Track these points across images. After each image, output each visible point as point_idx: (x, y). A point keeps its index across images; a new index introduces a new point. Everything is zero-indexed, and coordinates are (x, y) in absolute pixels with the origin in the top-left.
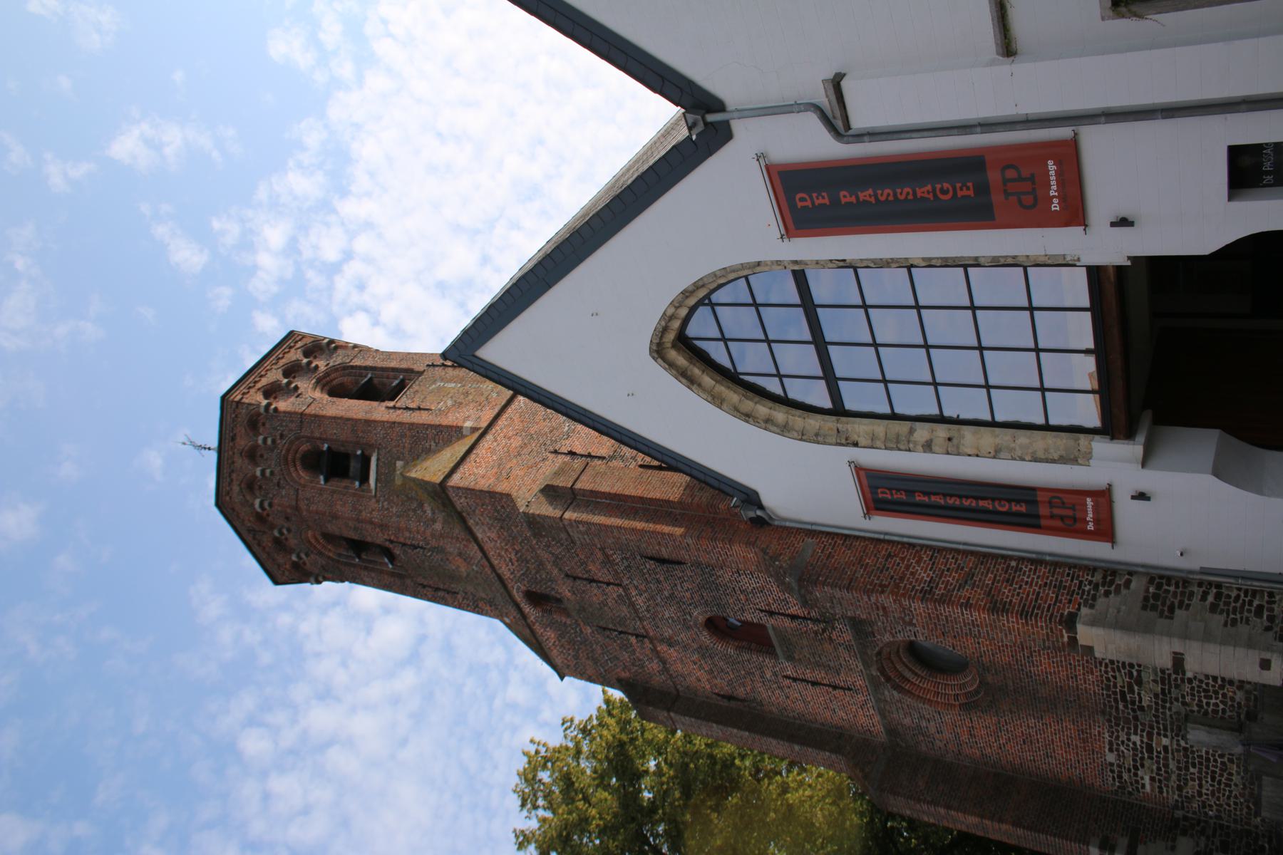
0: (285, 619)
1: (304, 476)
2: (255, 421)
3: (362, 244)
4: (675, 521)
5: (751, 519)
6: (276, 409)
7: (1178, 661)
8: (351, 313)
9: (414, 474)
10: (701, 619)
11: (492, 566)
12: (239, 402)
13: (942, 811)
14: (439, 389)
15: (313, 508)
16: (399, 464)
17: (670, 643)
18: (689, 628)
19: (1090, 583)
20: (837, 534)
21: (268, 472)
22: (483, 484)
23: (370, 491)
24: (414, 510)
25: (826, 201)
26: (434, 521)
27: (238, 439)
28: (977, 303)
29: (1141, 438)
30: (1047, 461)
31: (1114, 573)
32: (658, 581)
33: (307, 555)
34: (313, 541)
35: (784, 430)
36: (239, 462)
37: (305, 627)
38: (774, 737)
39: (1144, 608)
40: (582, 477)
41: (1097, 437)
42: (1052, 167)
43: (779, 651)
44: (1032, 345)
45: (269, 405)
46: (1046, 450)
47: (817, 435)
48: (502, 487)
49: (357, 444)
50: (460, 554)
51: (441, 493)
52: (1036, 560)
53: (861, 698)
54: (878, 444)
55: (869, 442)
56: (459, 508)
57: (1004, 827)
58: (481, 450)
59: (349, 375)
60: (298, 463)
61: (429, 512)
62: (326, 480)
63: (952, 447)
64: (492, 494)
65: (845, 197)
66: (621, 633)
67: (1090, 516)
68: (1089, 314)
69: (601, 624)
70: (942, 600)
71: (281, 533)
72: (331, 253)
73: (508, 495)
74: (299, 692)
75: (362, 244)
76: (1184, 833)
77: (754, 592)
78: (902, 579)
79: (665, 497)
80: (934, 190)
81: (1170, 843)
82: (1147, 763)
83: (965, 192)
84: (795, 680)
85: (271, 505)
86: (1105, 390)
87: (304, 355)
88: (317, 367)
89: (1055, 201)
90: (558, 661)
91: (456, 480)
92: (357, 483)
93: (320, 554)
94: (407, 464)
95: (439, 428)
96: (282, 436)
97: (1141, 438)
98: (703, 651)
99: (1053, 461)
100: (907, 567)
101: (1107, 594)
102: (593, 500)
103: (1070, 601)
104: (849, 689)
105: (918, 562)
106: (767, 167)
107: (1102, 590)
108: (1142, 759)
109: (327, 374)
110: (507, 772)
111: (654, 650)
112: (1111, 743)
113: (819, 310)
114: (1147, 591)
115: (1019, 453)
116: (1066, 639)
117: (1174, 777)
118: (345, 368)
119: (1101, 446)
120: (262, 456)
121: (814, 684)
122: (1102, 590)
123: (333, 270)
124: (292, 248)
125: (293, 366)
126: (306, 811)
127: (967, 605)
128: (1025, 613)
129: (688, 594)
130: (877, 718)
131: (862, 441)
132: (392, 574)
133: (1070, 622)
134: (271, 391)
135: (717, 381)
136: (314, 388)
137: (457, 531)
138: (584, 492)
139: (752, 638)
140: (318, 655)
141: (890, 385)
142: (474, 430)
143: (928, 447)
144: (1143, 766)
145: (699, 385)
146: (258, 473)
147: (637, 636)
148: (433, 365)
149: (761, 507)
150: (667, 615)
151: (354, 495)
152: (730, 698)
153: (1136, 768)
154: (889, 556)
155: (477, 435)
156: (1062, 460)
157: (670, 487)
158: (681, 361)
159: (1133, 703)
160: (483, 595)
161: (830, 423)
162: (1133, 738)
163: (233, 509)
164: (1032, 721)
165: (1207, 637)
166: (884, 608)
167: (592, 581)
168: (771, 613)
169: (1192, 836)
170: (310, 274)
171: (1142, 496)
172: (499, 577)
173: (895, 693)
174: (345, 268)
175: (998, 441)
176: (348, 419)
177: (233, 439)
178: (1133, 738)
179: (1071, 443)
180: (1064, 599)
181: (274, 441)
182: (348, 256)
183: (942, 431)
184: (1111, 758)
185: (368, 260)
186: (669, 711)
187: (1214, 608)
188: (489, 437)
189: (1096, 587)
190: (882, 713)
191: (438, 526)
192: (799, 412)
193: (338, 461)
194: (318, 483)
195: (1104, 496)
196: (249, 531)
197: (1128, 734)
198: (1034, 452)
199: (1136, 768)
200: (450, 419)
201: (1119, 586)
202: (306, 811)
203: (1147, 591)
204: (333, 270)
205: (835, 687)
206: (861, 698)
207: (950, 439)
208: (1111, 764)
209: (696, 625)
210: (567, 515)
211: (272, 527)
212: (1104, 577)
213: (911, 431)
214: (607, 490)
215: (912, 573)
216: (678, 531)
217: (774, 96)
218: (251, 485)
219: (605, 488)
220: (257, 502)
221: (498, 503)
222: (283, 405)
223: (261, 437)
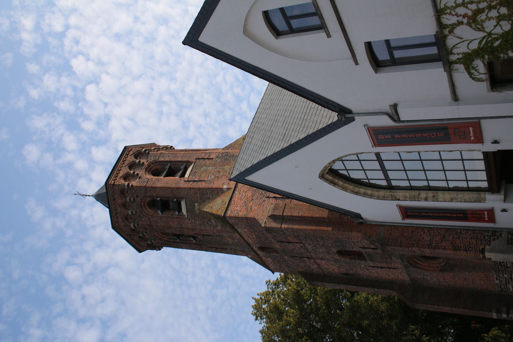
0: (74, 212)
1: (151, 211)
2: (123, 191)
3: (73, 20)
4: (327, 225)
5: (359, 223)
6: (132, 185)
8: (75, 56)
9: (206, 209)
10: (335, 251)
11: (244, 240)
12: (114, 184)
13: (436, 307)
14: (205, 170)
15: (159, 224)
16: (196, 204)
17: (322, 259)
18: (330, 254)
19: (488, 236)
20: (392, 226)
21: (134, 212)
22: (242, 214)
23: (185, 216)
24: (207, 222)
25: (390, 137)
26: (217, 226)
27: (117, 200)
28: (443, 158)
29: (503, 192)
30: (470, 202)
31: (495, 232)
32: (318, 241)
33: (154, 240)
34: (157, 235)
35: (371, 196)
36: (119, 209)
37: (84, 215)
38: (367, 287)
39: (508, 244)
40: (285, 210)
41: (487, 193)
42: (471, 129)
43: (367, 259)
44: (463, 169)
45: (129, 184)
46: (469, 198)
47: (384, 197)
48: (251, 215)
49: (175, 198)
50: (230, 237)
51: (223, 219)
52: (467, 229)
53: (400, 271)
54: (408, 199)
55: (404, 199)
56: (231, 223)
57: (460, 310)
58: (236, 199)
59: (159, 165)
60: (146, 206)
61: (214, 223)
62: (162, 213)
63: (435, 199)
64: (247, 219)
65: (396, 136)
66: (301, 257)
67: (486, 216)
68: (483, 161)
69: (292, 255)
70: (436, 247)
71: (143, 234)
72: (58, 27)
73: (254, 219)
74: (89, 246)
75: (73, 20)
77: (356, 241)
78: (419, 241)
79: (321, 216)
80: (429, 135)
82: (510, 282)
83: (440, 135)
84: (373, 267)
85: (138, 225)
86: (489, 179)
87: (135, 157)
88: (143, 163)
89: (472, 137)
90: (272, 268)
91: (229, 213)
92: (177, 213)
93: (161, 239)
94: (200, 204)
95: (212, 189)
96: (137, 196)
97: (503, 192)
98: (336, 261)
99: (472, 202)
100: (420, 235)
101: (494, 239)
102: (292, 219)
103: (481, 244)
104: (395, 268)
105: (424, 233)
106: (368, 128)
107: (492, 238)
108: (508, 281)
109: (149, 166)
111: (315, 262)
112: (497, 278)
113: (384, 162)
114: (508, 237)
115: (459, 200)
116: (481, 256)
118: (156, 162)
119: (489, 196)
120: (129, 205)
121: (381, 268)
122: (492, 238)
123: (61, 36)
124: (37, 28)
125: (132, 164)
126: (103, 300)
127: (445, 249)
128: (466, 250)
129: (330, 244)
130: (406, 276)
131: (401, 199)
132: (196, 244)
133: (483, 251)
134: (126, 177)
135: (344, 183)
136: (146, 173)
137: (228, 229)
138: (287, 216)
139: (358, 256)
140: (94, 227)
141: (407, 172)
142: (228, 189)
143: (426, 199)
144: (509, 283)
145: (338, 185)
146: (130, 213)
147: (308, 258)
148: (198, 159)
149: (362, 218)
150: (321, 251)
151: (177, 218)
152: (347, 274)
153: (506, 284)
154: (413, 232)
155: (231, 192)
156: (475, 201)
157: (324, 213)
158: (330, 178)
159: (504, 266)
160: (239, 249)
161: (387, 193)
162: (505, 276)
163: (120, 228)
164: (467, 273)
166: (414, 251)
167: (289, 243)
168: (365, 248)
170: (50, 39)
171: (504, 210)
172: (248, 244)
173: (414, 269)
174: (67, 33)
175: (451, 196)
176: (168, 188)
177: (114, 200)
178: (505, 276)
179: (478, 195)
181: (134, 199)
182: (67, 27)
183: (430, 194)
184: (497, 282)
185: (77, 28)
186: (322, 282)
188: (236, 192)
189: (490, 237)
190: (409, 275)
191: (219, 228)
192: (375, 189)
193: (166, 203)
194: (158, 214)
195: (491, 212)
196: (128, 235)
197: (503, 275)
198: (465, 199)
199: (506, 284)
200: (216, 185)
201: (498, 236)
202: (103, 300)
203: (508, 237)
204: (61, 36)
205: (390, 268)
206: (400, 271)
207: (434, 196)
208: (497, 284)
209: (333, 253)
210: (283, 226)
211: (139, 233)
212: (492, 233)
213: (419, 194)
214: (297, 215)
215: (422, 238)
216: (330, 229)
217: (371, 108)
218: (126, 218)
219: (295, 214)
220: (132, 225)
221: (251, 223)
222: (134, 183)
223: (128, 198)
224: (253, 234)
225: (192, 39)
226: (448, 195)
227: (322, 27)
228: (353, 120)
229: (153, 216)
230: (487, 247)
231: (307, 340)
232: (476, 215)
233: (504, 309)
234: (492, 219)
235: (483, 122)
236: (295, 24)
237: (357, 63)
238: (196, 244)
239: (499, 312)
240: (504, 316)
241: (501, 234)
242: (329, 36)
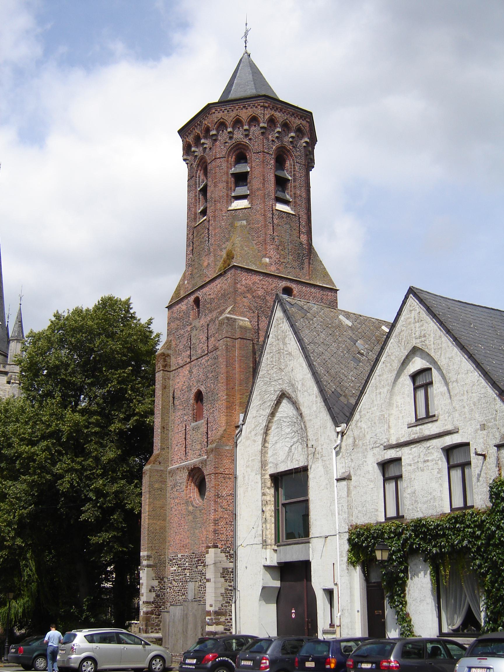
7: (208, 580)
39: (223, 569)
66: (190, 348)
70: (216, 502)
76: (159, 582)
81: (154, 578)
101: (227, 556)
108: (181, 567)
110: (106, 294)
112: (184, 556)
117: (177, 577)
127: (215, 511)
128: (215, 531)
129: (209, 385)
133: (216, 547)
144: (179, 567)
153: (178, 565)
165: (216, 588)
169: (159, 585)
178: (187, 563)
180: (223, 543)
184: (179, 556)
187: (227, 589)
209: (199, 386)
224: (215, 296)
225: (412, 291)
227: (419, 421)
231: (64, 312)
233: (151, 563)
236: (421, 393)
239: (149, 557)
240: (145, 563)
241: (232, 562)
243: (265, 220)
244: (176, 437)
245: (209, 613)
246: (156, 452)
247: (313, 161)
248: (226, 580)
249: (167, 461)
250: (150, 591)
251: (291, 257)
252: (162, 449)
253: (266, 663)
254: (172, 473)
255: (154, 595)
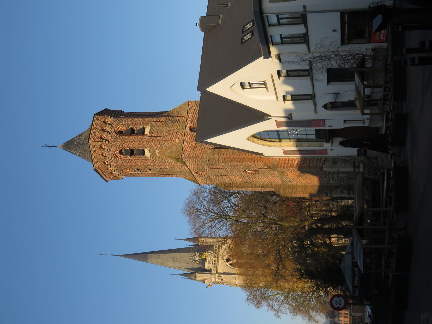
7: (338, 170)
26: (171, 163)
27: (97, 151)
29: (331, 142)
52: (314, 158)
133: (322, 168)
167: (217, 168)
171: (331, 150)
184: (326, 179)
195: (326, 150)
226: (307, 144)
227: (266, 87)
228: (271, 118)
229: (124, 159)
230: (324, 166)
232: (321, 152)
233: (329, 192)
234: (326, 153)
235: (326, 121)
237: (278, 100)
238: (151, 173)
242: (268, 91)
243: (155, 141)
244: (267, 181)
245: (354, 170)
246: (273, 190)
247: (118, 111)
248: (338, 162)
249: (277, 185)
250: (343, 193)
251: (174, 127)
252: (272, 187)
253: (390, 77)
254: (283, 182)
255: (345, 191)
